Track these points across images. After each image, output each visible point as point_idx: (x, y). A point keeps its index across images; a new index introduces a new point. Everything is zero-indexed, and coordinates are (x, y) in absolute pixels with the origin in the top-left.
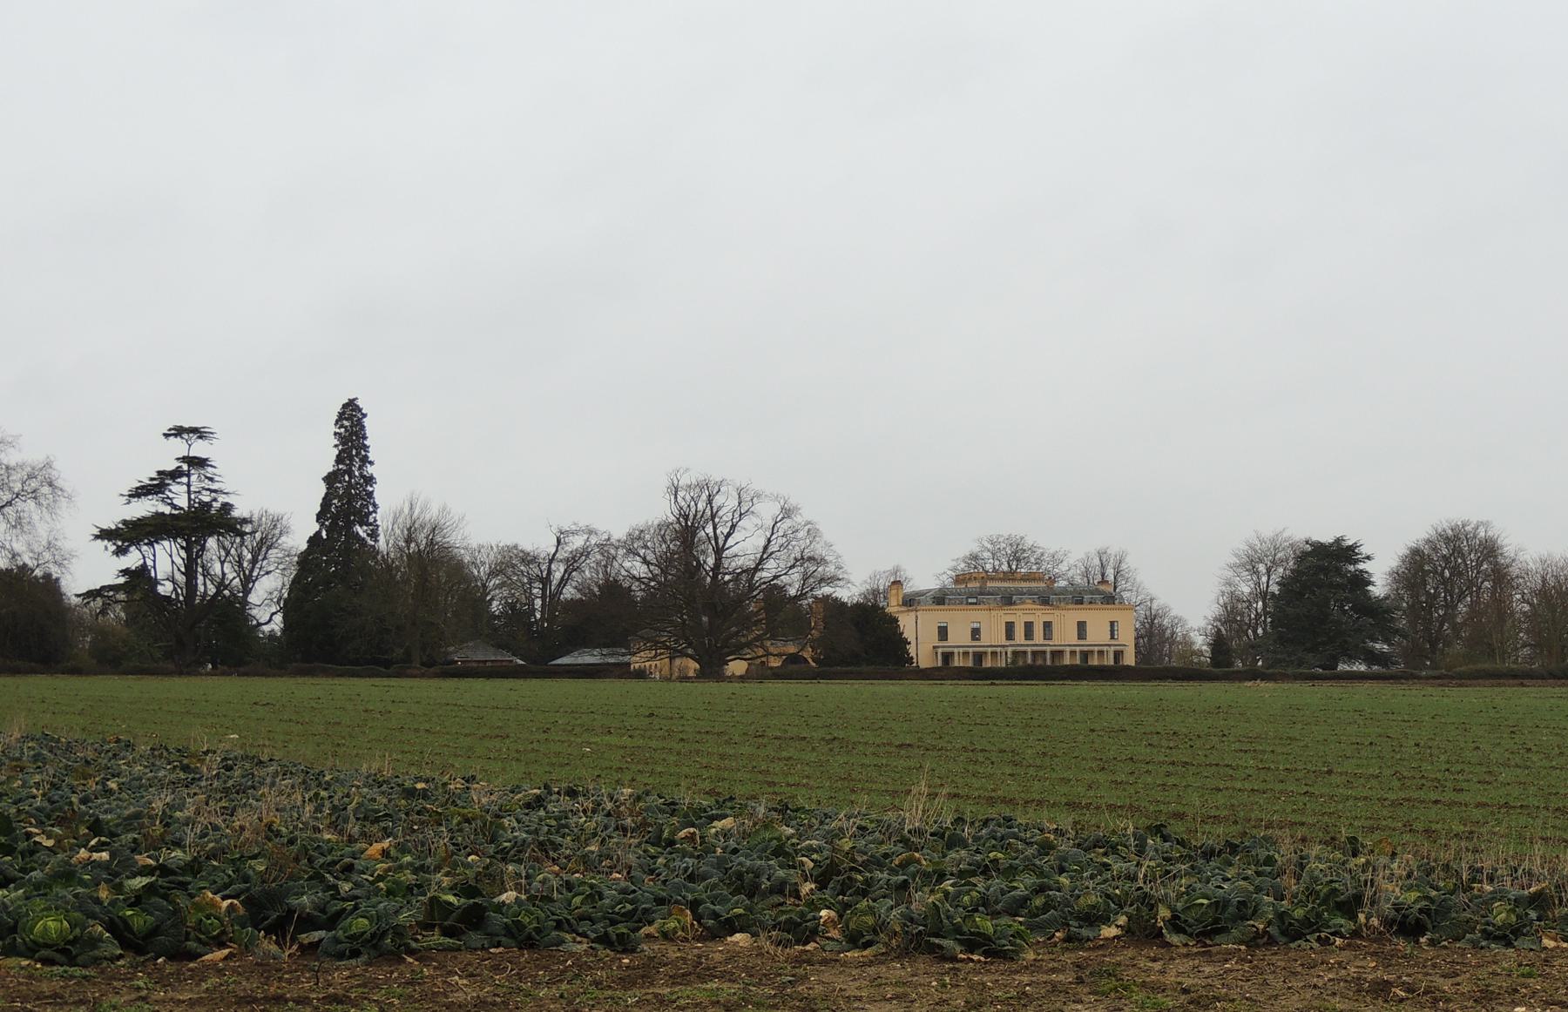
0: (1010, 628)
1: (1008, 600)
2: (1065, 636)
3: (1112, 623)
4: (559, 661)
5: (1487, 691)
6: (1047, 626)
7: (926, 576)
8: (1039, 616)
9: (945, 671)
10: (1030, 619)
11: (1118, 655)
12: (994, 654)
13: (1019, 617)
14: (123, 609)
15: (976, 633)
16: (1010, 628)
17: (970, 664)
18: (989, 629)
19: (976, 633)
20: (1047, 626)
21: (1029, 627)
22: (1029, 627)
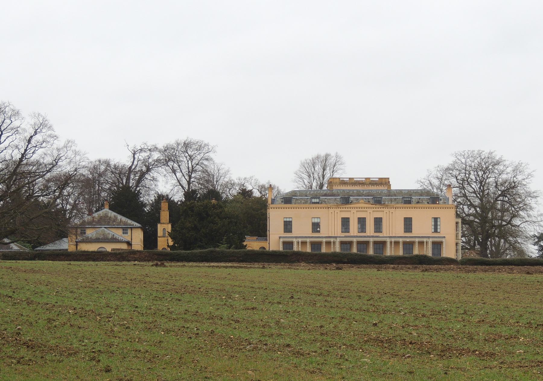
0: (345, 222)
1: (346, 201)
2: (393, 228)
3: (436, 220)
4: (39, 248)
5: (481, 275)
6: (378, 222)
7: (287, 185)
8: (371, 215)
9: (287, 257)
10: (362, 215)
11: (437, 245)
12: (421, 243)
13: (353, 214)
14: (61, 208)
15: (316, 227)
16: (345, 222)
17: (401, 253)
18: (332, 226)
19: (316, 227)
20: (378, 222)
21: (362, 222)
22: (362, 222)
